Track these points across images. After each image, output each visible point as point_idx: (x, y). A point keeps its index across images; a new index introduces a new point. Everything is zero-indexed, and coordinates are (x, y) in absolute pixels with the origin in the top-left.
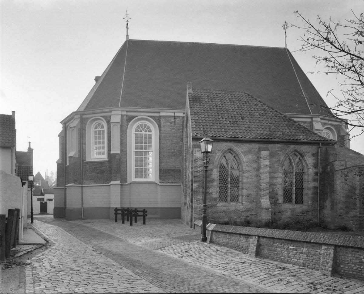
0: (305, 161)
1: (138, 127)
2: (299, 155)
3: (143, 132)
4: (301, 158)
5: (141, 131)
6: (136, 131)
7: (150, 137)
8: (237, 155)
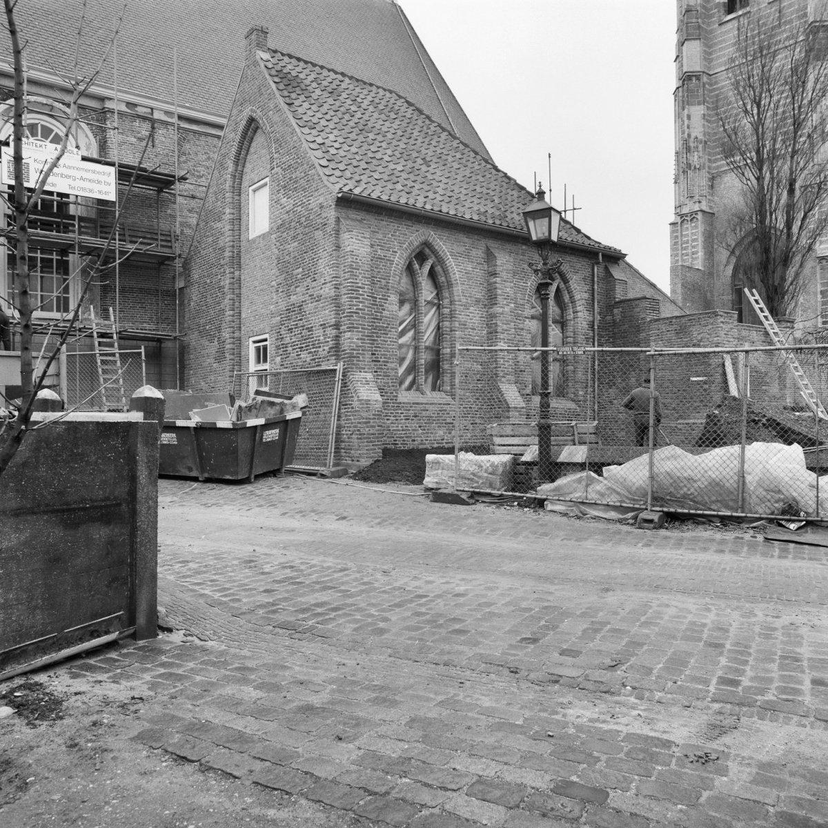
0: (570, 292)
2: (558, 277)
4: (562, 285)
8: (440, 261)
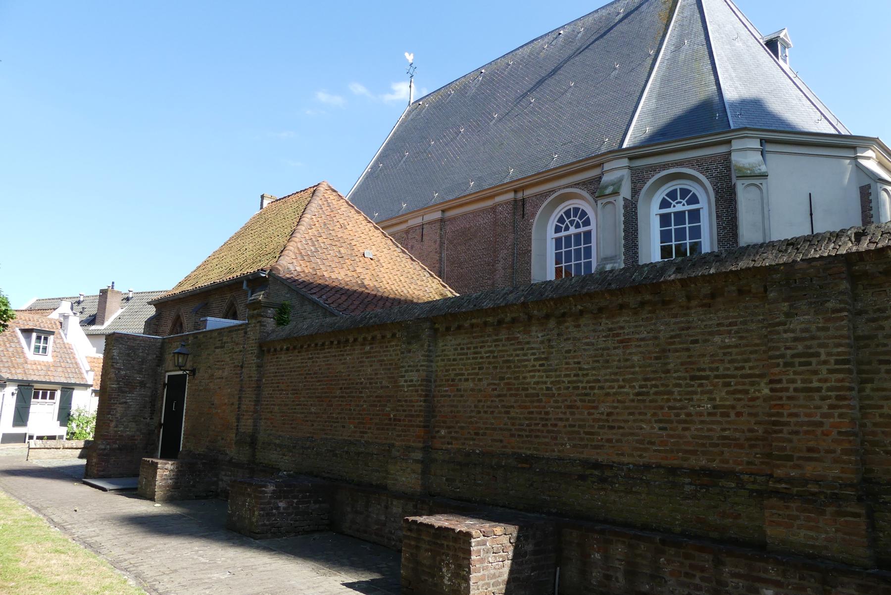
1: (561, 220)
3: (573, 230)
5: (567, 229)
6: (558, 229)
7: (695, 215)
